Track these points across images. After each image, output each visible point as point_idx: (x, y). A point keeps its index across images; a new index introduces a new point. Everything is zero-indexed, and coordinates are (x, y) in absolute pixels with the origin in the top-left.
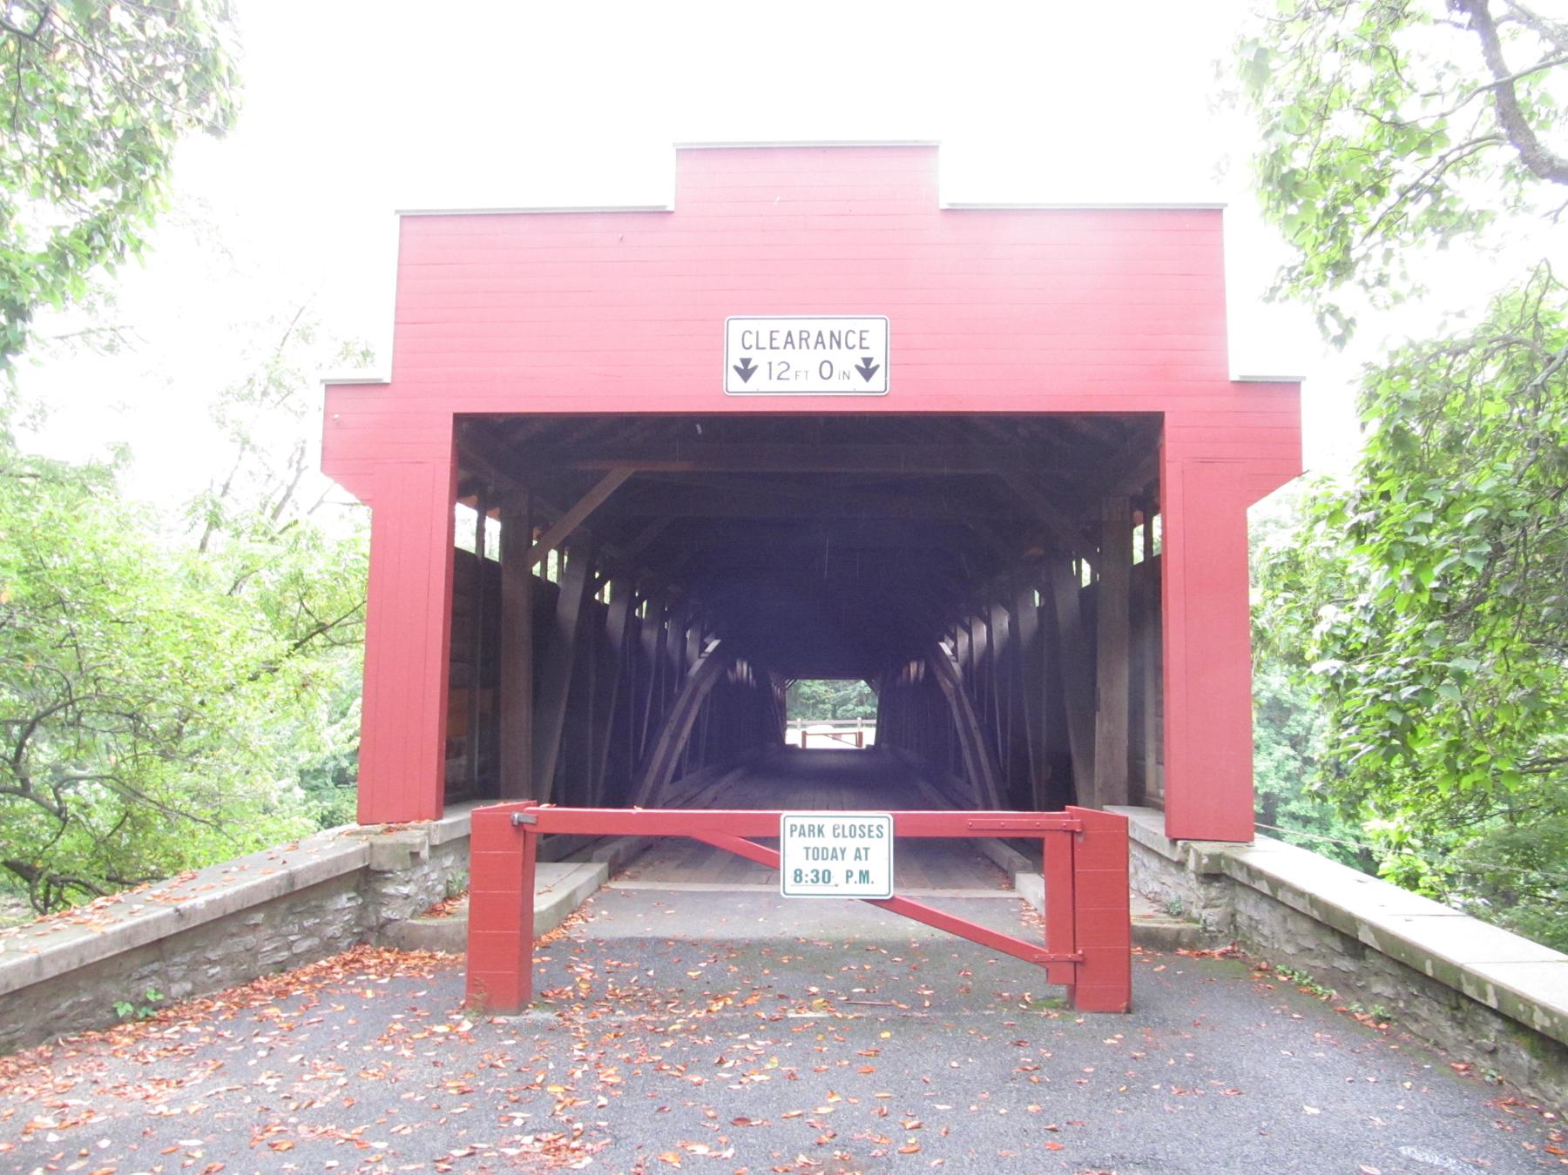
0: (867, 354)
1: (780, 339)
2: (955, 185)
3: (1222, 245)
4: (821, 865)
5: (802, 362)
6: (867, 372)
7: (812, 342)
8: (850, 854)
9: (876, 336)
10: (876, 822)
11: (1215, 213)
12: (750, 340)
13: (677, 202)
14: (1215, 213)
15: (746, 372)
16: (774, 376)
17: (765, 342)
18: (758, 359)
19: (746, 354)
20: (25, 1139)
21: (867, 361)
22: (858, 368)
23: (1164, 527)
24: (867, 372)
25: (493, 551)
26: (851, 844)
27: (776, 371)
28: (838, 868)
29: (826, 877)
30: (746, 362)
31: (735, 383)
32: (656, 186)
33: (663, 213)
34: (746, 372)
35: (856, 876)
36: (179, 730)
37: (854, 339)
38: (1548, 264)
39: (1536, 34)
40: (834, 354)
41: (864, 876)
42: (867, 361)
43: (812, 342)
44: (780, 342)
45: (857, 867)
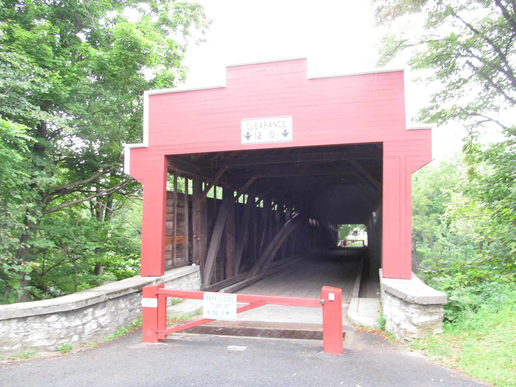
0: (285, 129)
1: (258, 125)
2: (313, 71)
3: (130, 166)
5: (267, 132)
6: (285, 134)
9: (288, 122)
11: (401, 72)
14: (401, 72)
15: (248, 137)
16: (257, 138)
21: (285, 131)
23: (238, 353)
24: (285, 134)
25: (191, 192)
27: (257, 135)
30: (248, 134)
32: (220, 80)
34: (248, 137)
35: (225, 313)
36: (501, 54)
39: (509, 64)
42: (285, 131)
44: (258, 127)
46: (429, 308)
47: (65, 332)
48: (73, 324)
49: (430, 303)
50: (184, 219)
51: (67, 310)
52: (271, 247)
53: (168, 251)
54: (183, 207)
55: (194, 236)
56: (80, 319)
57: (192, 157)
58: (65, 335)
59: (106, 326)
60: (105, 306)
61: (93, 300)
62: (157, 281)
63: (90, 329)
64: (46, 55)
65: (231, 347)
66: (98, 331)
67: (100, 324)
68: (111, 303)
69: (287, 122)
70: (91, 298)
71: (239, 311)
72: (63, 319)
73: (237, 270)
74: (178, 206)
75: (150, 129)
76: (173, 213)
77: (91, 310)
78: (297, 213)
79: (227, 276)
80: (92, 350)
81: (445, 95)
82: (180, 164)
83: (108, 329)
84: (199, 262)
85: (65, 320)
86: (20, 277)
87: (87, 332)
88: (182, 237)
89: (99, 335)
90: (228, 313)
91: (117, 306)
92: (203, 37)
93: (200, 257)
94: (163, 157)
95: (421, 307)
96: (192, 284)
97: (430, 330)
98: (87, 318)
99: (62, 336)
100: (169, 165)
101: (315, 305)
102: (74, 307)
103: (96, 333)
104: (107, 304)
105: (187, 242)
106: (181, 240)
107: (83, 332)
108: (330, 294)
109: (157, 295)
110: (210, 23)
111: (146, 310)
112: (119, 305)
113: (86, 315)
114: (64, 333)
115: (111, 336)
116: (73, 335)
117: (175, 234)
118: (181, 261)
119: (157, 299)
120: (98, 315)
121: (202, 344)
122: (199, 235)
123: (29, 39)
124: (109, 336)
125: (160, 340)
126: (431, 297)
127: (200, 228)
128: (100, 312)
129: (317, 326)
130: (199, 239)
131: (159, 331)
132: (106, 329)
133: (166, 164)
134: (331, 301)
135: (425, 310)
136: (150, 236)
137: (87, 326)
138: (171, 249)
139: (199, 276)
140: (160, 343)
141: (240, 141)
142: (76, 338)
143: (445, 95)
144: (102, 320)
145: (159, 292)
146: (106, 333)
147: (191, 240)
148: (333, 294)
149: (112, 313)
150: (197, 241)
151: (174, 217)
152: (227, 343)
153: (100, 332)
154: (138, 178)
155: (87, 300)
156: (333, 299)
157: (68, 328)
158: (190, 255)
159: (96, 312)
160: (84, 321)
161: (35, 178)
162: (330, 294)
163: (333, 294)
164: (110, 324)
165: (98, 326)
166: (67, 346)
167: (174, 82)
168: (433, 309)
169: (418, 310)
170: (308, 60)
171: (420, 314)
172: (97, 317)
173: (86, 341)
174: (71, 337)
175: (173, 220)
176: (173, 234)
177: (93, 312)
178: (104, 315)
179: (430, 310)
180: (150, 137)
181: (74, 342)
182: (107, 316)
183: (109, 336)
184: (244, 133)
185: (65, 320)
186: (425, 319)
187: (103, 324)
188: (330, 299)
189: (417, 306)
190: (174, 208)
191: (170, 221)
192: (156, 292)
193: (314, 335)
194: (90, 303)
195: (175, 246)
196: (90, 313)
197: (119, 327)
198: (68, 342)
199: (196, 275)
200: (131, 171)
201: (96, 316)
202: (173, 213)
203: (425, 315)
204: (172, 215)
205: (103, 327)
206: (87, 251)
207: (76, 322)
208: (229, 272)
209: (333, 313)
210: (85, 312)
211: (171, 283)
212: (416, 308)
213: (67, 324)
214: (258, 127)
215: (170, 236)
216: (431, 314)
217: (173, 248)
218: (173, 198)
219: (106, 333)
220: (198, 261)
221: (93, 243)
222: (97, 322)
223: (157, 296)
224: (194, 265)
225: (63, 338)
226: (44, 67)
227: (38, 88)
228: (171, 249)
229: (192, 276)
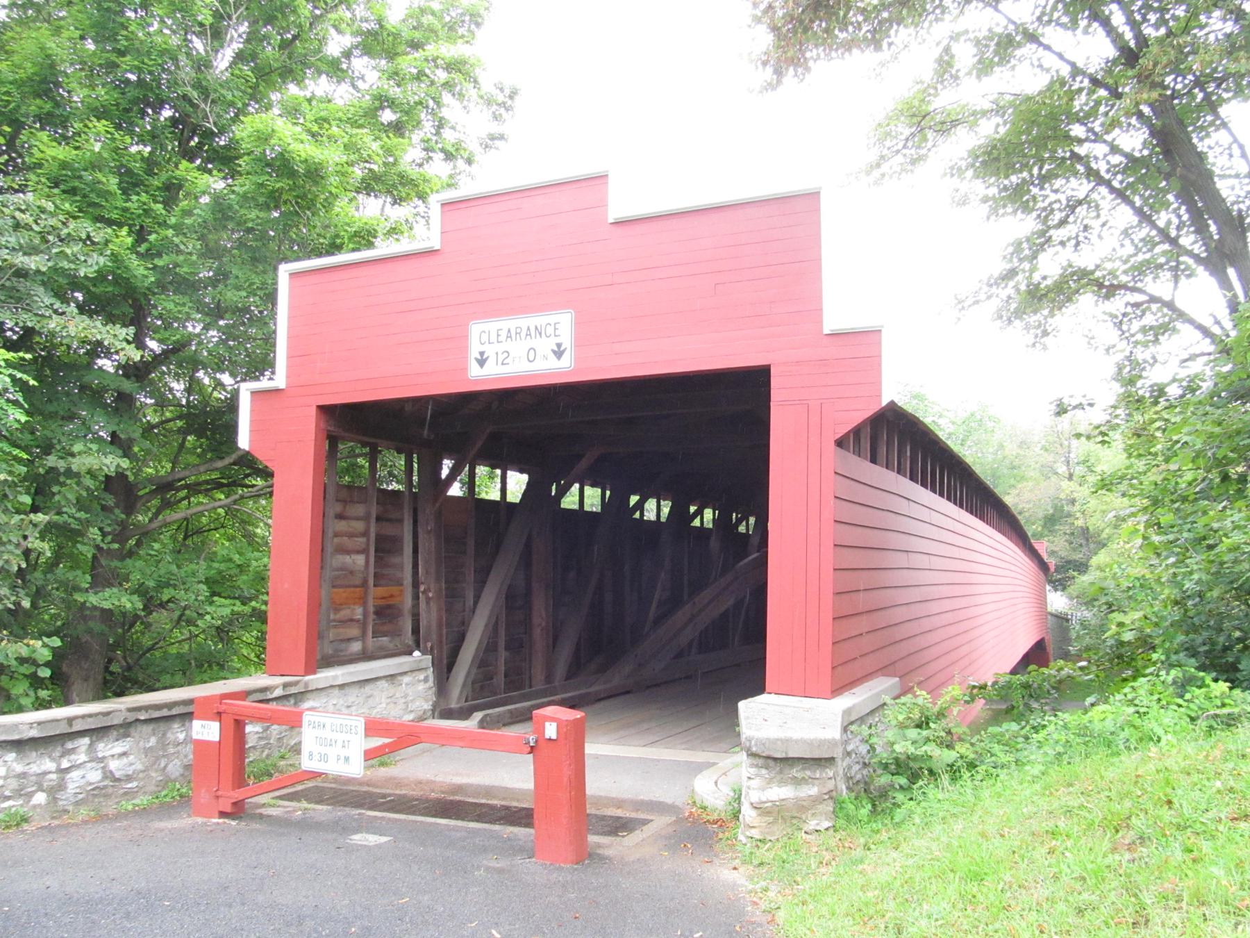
0: (558, 340)
1: (504, 334)
3: (251, 431)
4: (323, 750)
6: (559, 353)
7: (523, 334)
8: (340, 744)
9: (563, 324)
10: (354, 723)
12: (485, 338)
13: (442, 242)
17: (493, 338)
18: (490, 351)
19: (482, 348)
20: (1084, 664)
21: (559, 345)
22: (554, 352)
24: (559, 353)
26: (341, 737)
27: (501, 358)
28: (332, 752)
29: (324, 758)
30: (482, 354)
31: (475, 371)
33: (431, 252)
34: (482, 362)
35: (342, 760)
37: (550, 330)
38: (1241, 147)
40: (537, 343)
41: (347, 759)
42: (559, 345)
43: (523, 334)
44: (503, 338)
45: (344, 753)
46: (792, 766)
47: (14, 784)
48: (35, 769)
49: (791, 755)
50: (402, 549)
51: (16, 737)
52: (681, 616)
53: (352, 620)
54: (401, 521)
55: (422, 588)
56: (53, 760)
57: (408, 408)
58: (12, 791)
59: (129, 778)
60: (127, 735)
61: (90, 720)
62: (285, 686)
63: (83, 782)
64: (106, 194)
65: (358, 838)
66: (105, 787)
67: (111, 772)
68: (147, 729)
69: (563, 324)
70: (83, 717)
71: (369, 755)
72: (11, 756)
73: (561, 669)
74: (378, 519)
75: (289, 348)
76: (365, 534)
77: (86, 741)
78: (618, 535)
79: (533, 683)
80: (77, 825)
81: (1040, 241)
82: (358, 425)
83: (134, 784)
84: (432, 648)
85: (16, 760)
86: (26, 669)
87: (71, 787)
88: (395, 590)
89: (107, 796)
90: (347, 759)
91: (164, 735)
92: (495, 128)
93: (434, 637)
94: (313, 411)
95: (771, 763)
96: (406, 696)
97: (794, 821)
98: (73, 757)
99: (7, 793)
100: (332, 429)
101: (513, 747)
102: (34, 733)
103: (97, 792)
104: (132, 730)
105: (408, 602)
106: (392, 596)
107: (61, 786)
108: (547, 724)
109: (219, 714)
110: (511, 97)
111: (201, 745)
112: (169, 735)
113: (73, 751)
114: (12, 787)
115: (142, 800)
116: (33, 793)
117: (371, 582)
118: (391, 646)
119: (217, 724)
120: (107, 754)
121: (305, 825)
122: (432, 586)
123: (64, 165)
124: (137, 801)
125: (223, 814)
126: (797, 741)
127: (433, 570)
128: (109, 748)
129: (523, 792)
130: (431, 595)
131: (220, 793)
132: (130, 786)
133: (323, 425)
134: (550, 739)
135: (781, 772)
136: (286, 586)
137: (75, 775)
138: (360, 617)
139: (431, 679)
140: (221, 821)
141: (465, 369)
142: (40, 798)
143: (1040, 241)
144: (114, 765)
145: (223, 708)
146: (129, 794)
147: (416, 597)
148: (554, 725)
149: (147, 751)
150: (428, 600)
151: (368, 544)
152: (346, 829)
153: (110, 790)
154: (264, 457)
155: (70, 720)
156: (554, 736)
157: (23, 775)
158: (416, 631)
159: (101, 746)
160: (65, 764)
161: (70, 459)
162: (547, 724)
163: (554, 725)
164: (141, 775)
165: (105, 777)
166: (16, 813)
167: (377, 242)
168: (804, 769)
169: (764, 771)
170: (611, 180)
171: (770, 781)
172: (104, 758)
173: (70, 808)
174: (30, 795)
175: (364, 551)
176: (364, 584)
177: (90, 745)
178: (125, 754)
179: (795, 772)
180: (290, 367)
181: (35, 807)
182: (132, 757)
183: (137, 801)
184: (474, 353)
185: (16, 760)
186: (781, 792)
187: (118, 774)
188: (547, 736)
189: (760, 762)
190: (368, 523)
191: (358, 552)
192: (217, 707)
193: (521, 817)
194: (78, 727)
195: (371, 609)
196: (83, 749)
197: (166, 782)
198: (22, 806)
199: (422, 677)
200: (251, 441)
201: (100, 755)
202: (365, 534)
203: (782, 782)
204: (363, 540)
205: (119, 780)
206: (208, 617)
207: (45, 764)
208: (538, 673)
209: (563, 768)
210: (69, 745)
211: (336, 691)
212: (757, 766)
213: (19, 768)
214: (503, 338)
215: (356, 586)
216: (797, 782)
217: (365, 614)
218: (365, 502)
219: (129, 794)
220: (429, 645)
221: (227, 602)
222: (103, 768)
223: (219, 716)
224: (417, 653)
225: (8, 798)
226: (99, 219)
227: (73, 266)
228: (360, 617)
229: (406, 679)
